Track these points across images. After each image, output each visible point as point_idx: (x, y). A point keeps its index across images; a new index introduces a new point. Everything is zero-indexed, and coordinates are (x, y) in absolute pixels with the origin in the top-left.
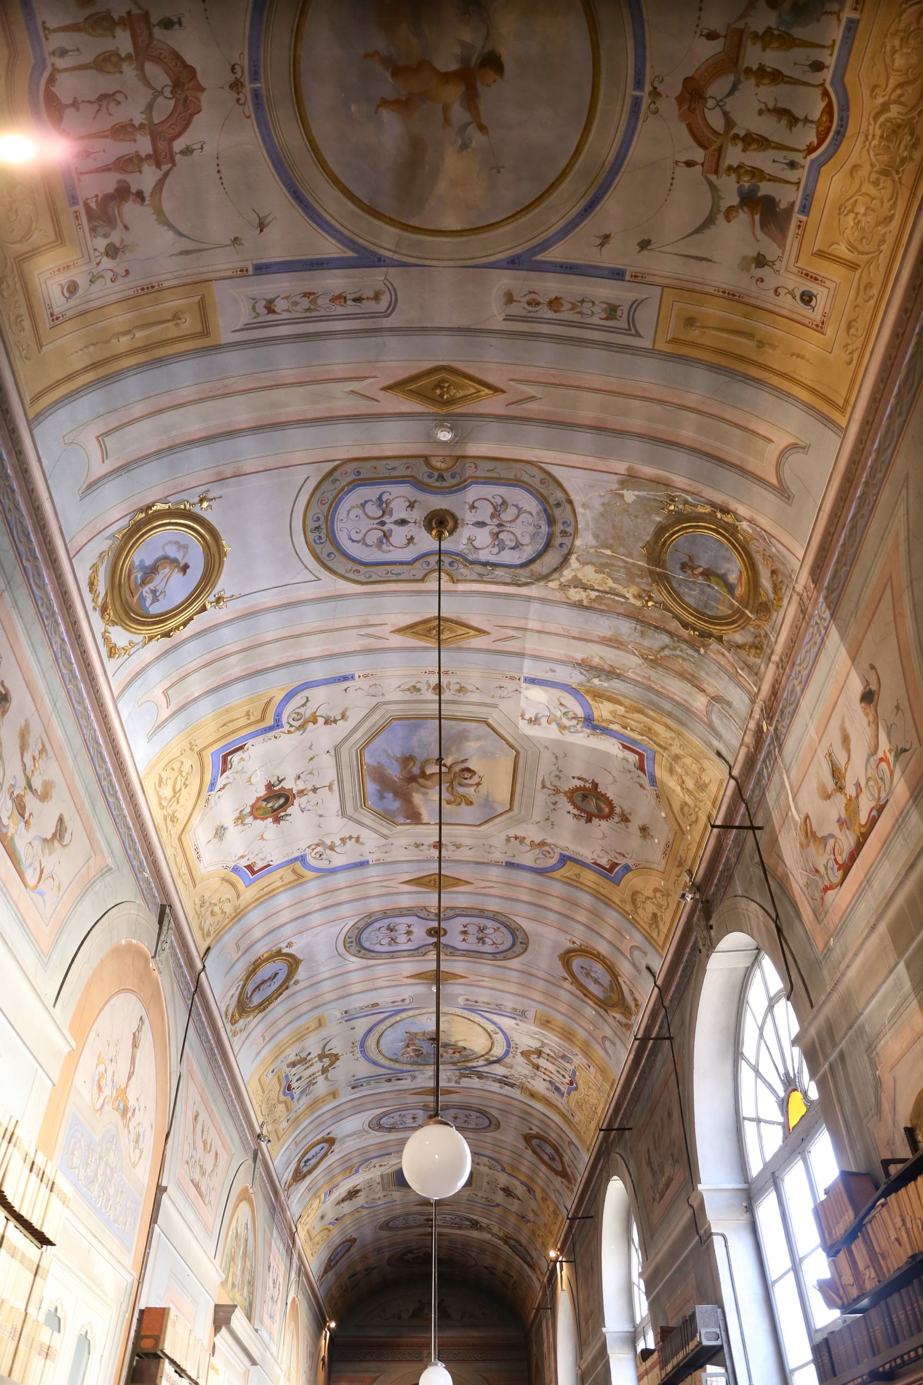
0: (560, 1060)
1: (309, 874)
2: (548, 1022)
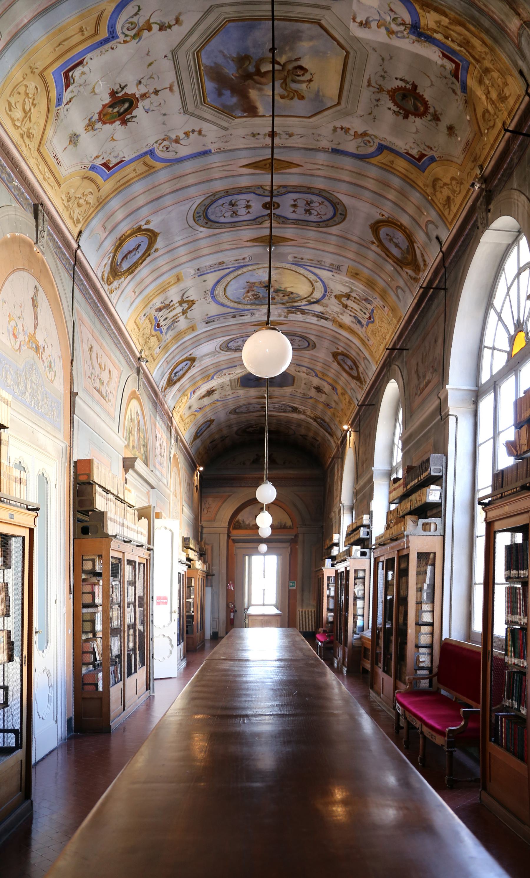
0: (363, 302)
1: (159, 165)
2: (357, 274)
